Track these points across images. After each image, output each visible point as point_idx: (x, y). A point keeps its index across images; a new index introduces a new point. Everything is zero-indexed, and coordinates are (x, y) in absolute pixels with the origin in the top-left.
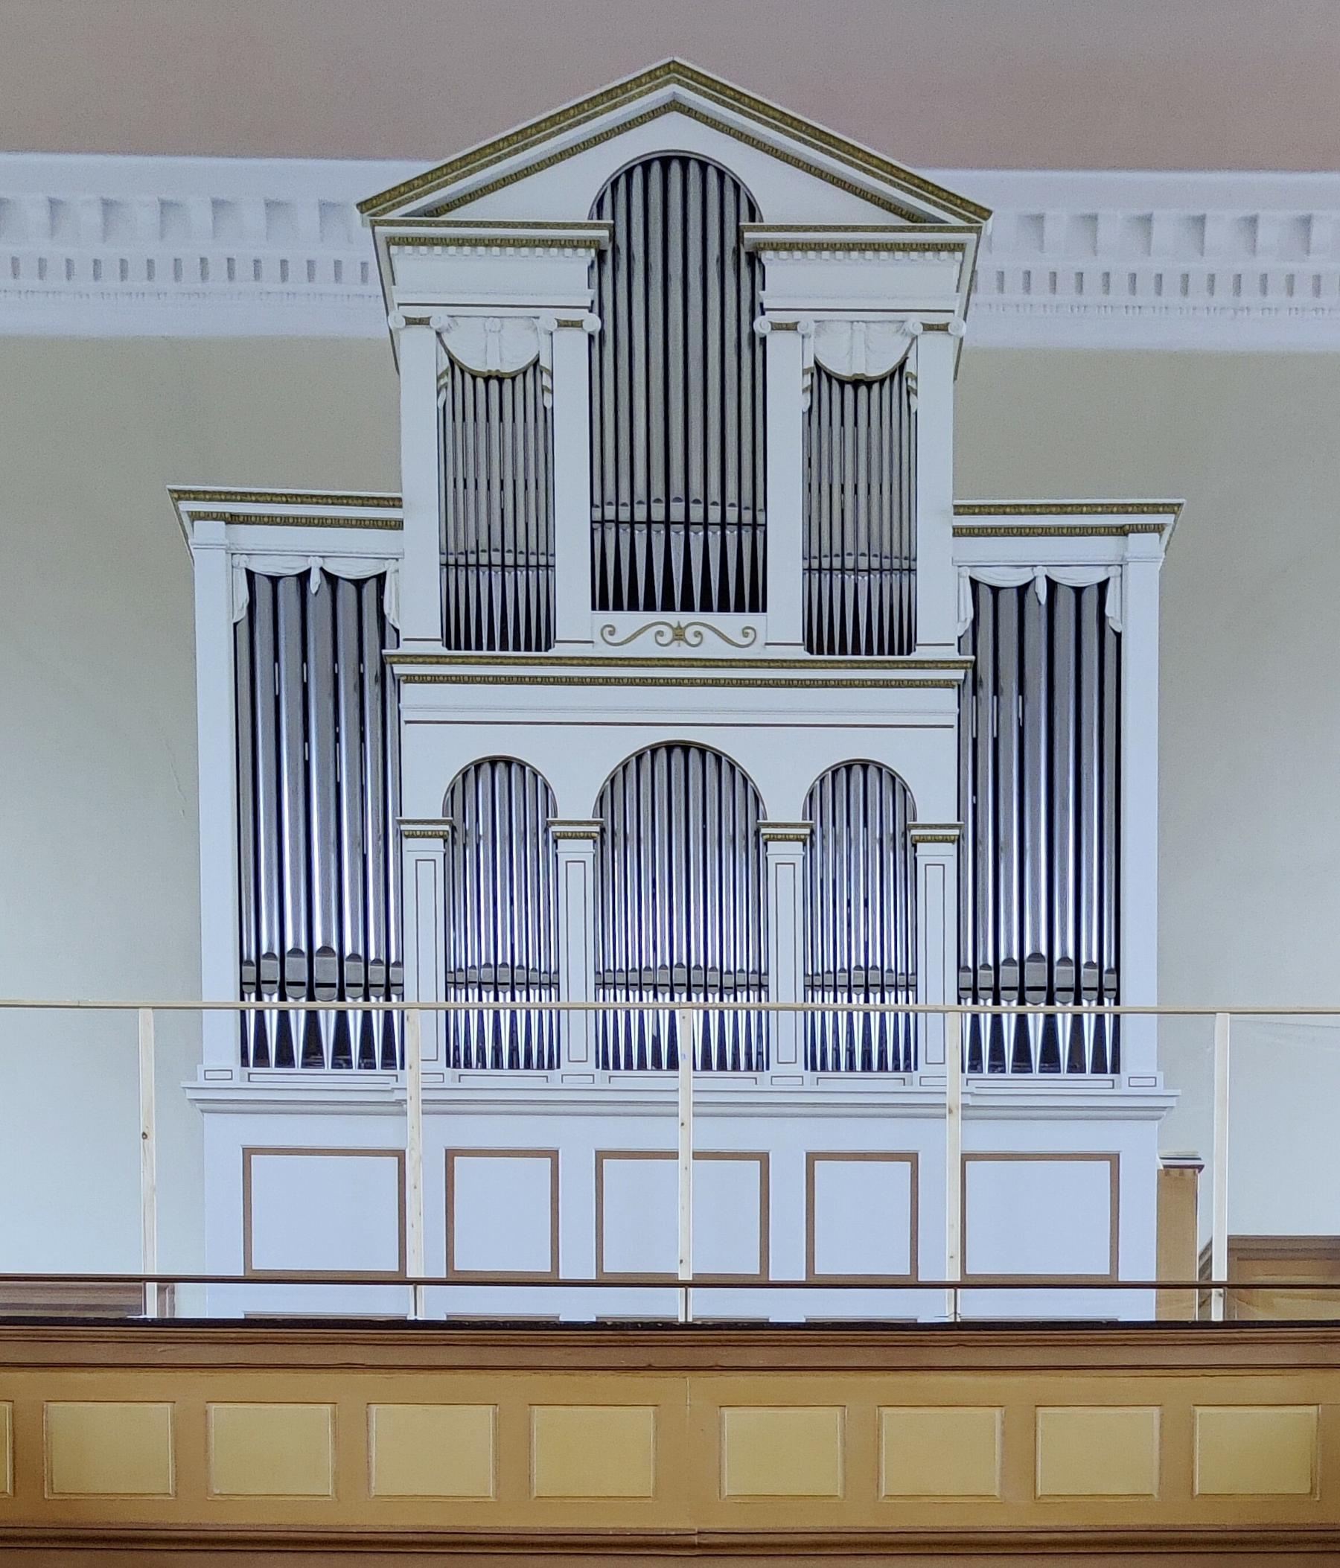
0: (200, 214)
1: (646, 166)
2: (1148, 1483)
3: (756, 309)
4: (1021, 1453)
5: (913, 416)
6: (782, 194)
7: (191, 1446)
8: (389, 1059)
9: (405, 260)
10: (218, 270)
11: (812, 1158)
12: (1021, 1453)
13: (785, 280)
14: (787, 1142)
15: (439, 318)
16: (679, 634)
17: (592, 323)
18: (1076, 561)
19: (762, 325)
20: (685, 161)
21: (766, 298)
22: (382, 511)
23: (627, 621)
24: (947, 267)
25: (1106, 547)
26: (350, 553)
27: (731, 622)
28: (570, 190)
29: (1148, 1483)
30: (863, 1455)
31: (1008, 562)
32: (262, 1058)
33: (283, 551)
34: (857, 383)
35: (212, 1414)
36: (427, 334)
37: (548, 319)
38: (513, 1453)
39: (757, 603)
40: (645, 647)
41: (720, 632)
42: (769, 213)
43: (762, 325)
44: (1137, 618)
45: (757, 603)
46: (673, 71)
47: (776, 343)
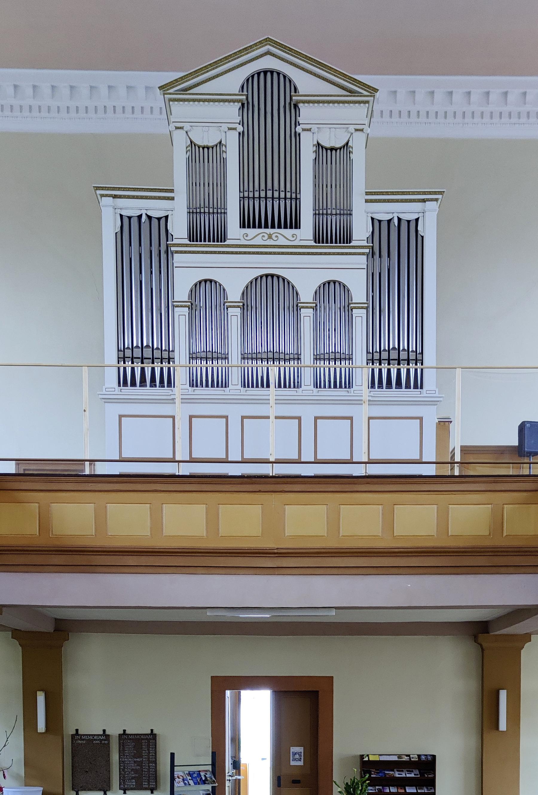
0: (104, 91)
1: (259, 74)
2: (433, 531)
3: (297, 124)
4: (389, 522)
5: (351, 161)
6: (306, 83)
7: (101, 519)
8: (169, 384)
9: (175, 106)
10: (110, 110)
11: (316, 418)
12: (389, 522)
13: (307, 113)
14: (307, 413)
15: (187, 126)
16: (270, 237)
17: (240, 128)
18: (408, 211)
19: (299, 129)
20: (272, 72)
21: (300, 120)
22: (167, 194)
23: (252, 232)
24: (362, 109)
25: (418, 206)
26: (156, 208)
27: (288, 232)
28: (232, 82)
29: (433, 531)
30: (334, 522)
31: (385, 211)
32: (125, 384)
33: (132, 207)
34: (332, 149)
35: (108, 507)
36: (182, 133)
37: (225, 127)
38: (212, 521)
39: (297, 225)
40: (258, 241)
41: (282, 236)
42: (302, 90)
43: (299, 129)
44: (429, 230)
45: (297, 225)
46: (268, 41)
47: (304, 135)
